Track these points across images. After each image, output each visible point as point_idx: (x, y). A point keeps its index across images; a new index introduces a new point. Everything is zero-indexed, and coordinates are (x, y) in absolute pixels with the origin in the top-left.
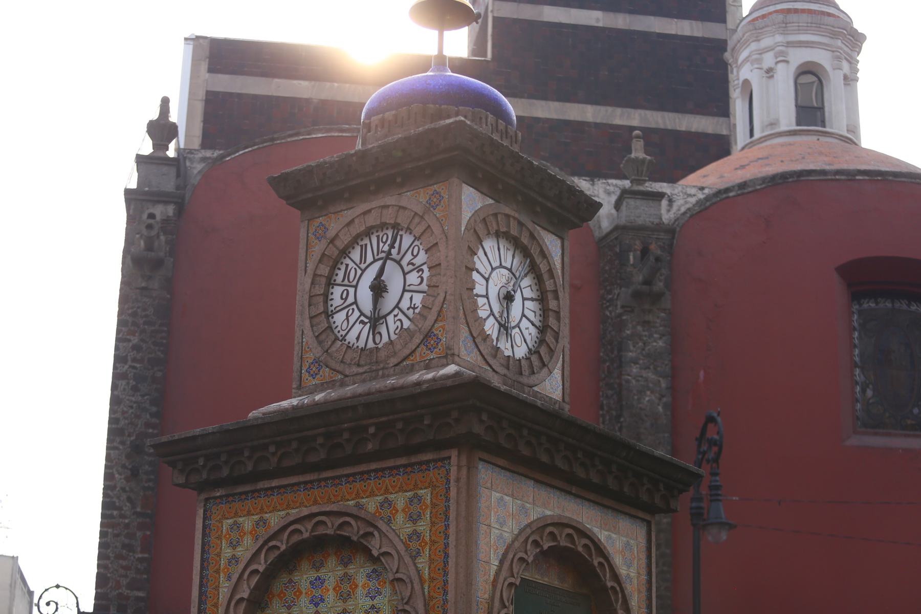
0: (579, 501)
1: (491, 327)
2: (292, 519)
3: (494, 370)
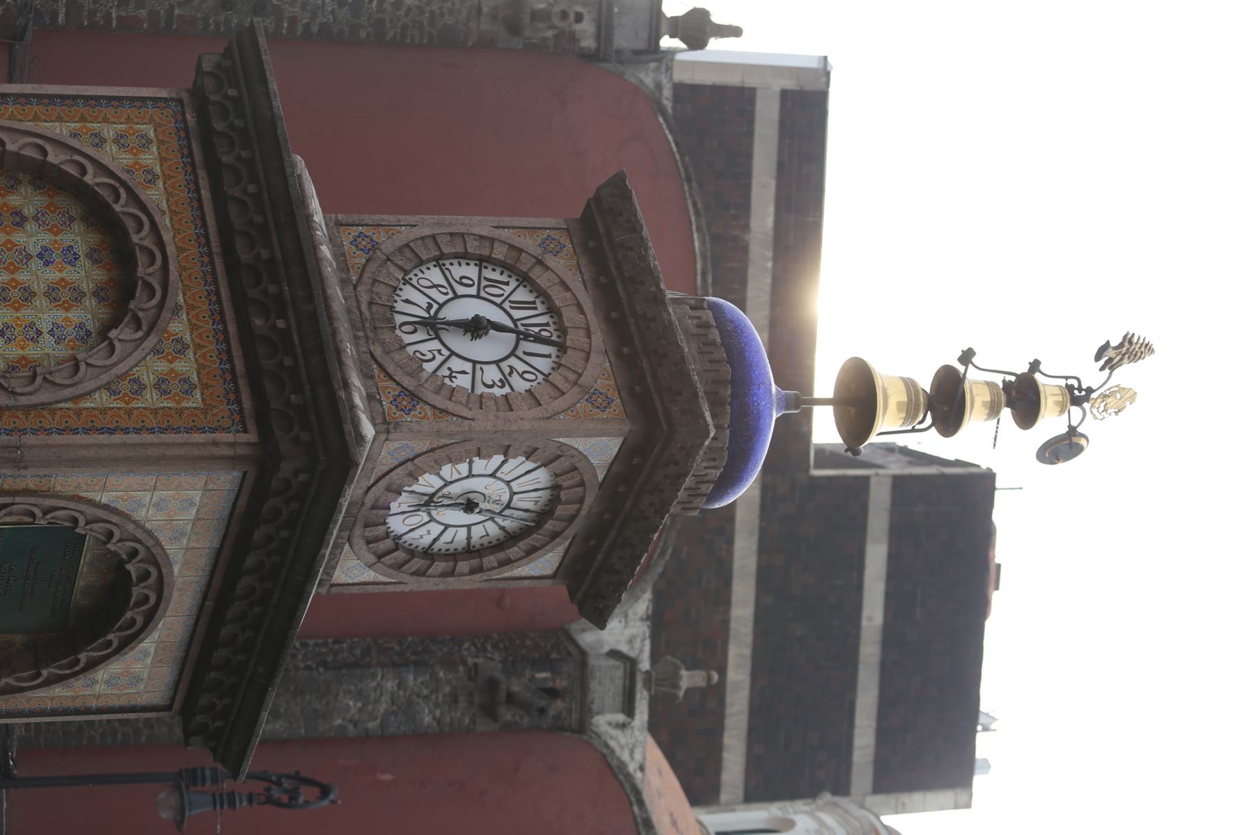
0: (195, 610)
1: (428, 483)
2: (157, 218)
3: (369, 488)
